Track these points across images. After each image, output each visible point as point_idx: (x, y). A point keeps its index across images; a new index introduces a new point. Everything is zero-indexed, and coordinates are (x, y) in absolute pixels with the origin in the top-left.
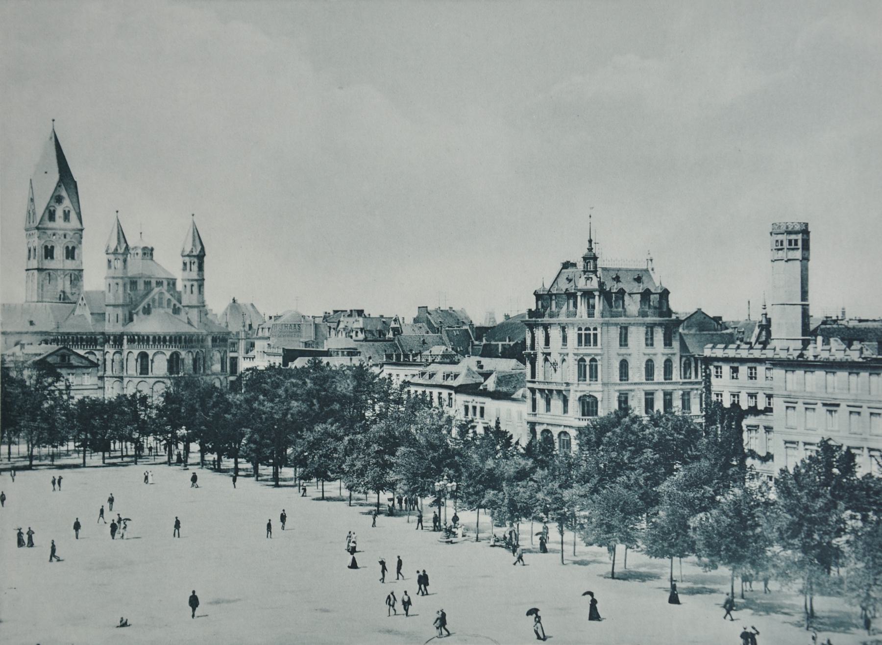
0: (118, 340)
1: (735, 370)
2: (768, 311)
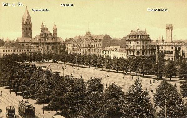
0: (43, 44)
1: (162, 47)
2: (55, 23)
